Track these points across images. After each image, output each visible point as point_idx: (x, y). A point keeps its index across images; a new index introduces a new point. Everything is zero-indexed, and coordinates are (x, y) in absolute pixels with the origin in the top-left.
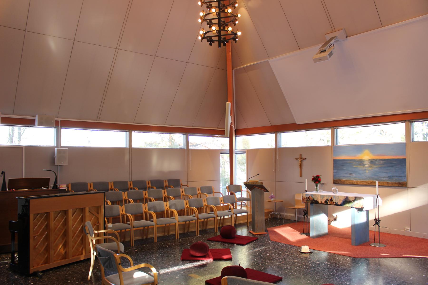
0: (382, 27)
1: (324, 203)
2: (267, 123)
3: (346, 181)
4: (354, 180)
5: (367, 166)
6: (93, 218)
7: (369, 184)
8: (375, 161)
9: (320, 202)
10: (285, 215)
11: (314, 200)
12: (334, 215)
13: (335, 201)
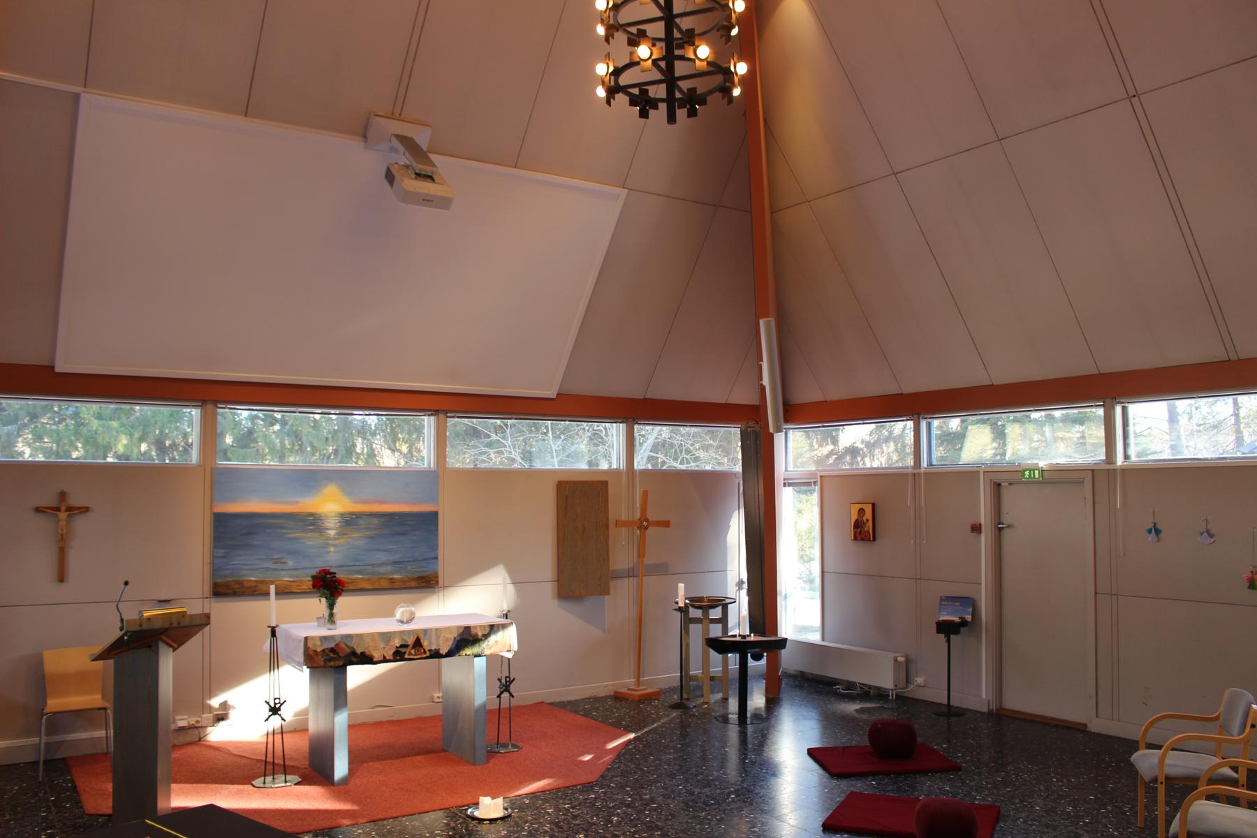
0: (515, 167)
1: (392, 658)
3: (259, 585)
4: (290, 577)
5: (332, 533)
8: (357, 518)
11: (354, 653)
12: (215, 702)
13: (430, 644)
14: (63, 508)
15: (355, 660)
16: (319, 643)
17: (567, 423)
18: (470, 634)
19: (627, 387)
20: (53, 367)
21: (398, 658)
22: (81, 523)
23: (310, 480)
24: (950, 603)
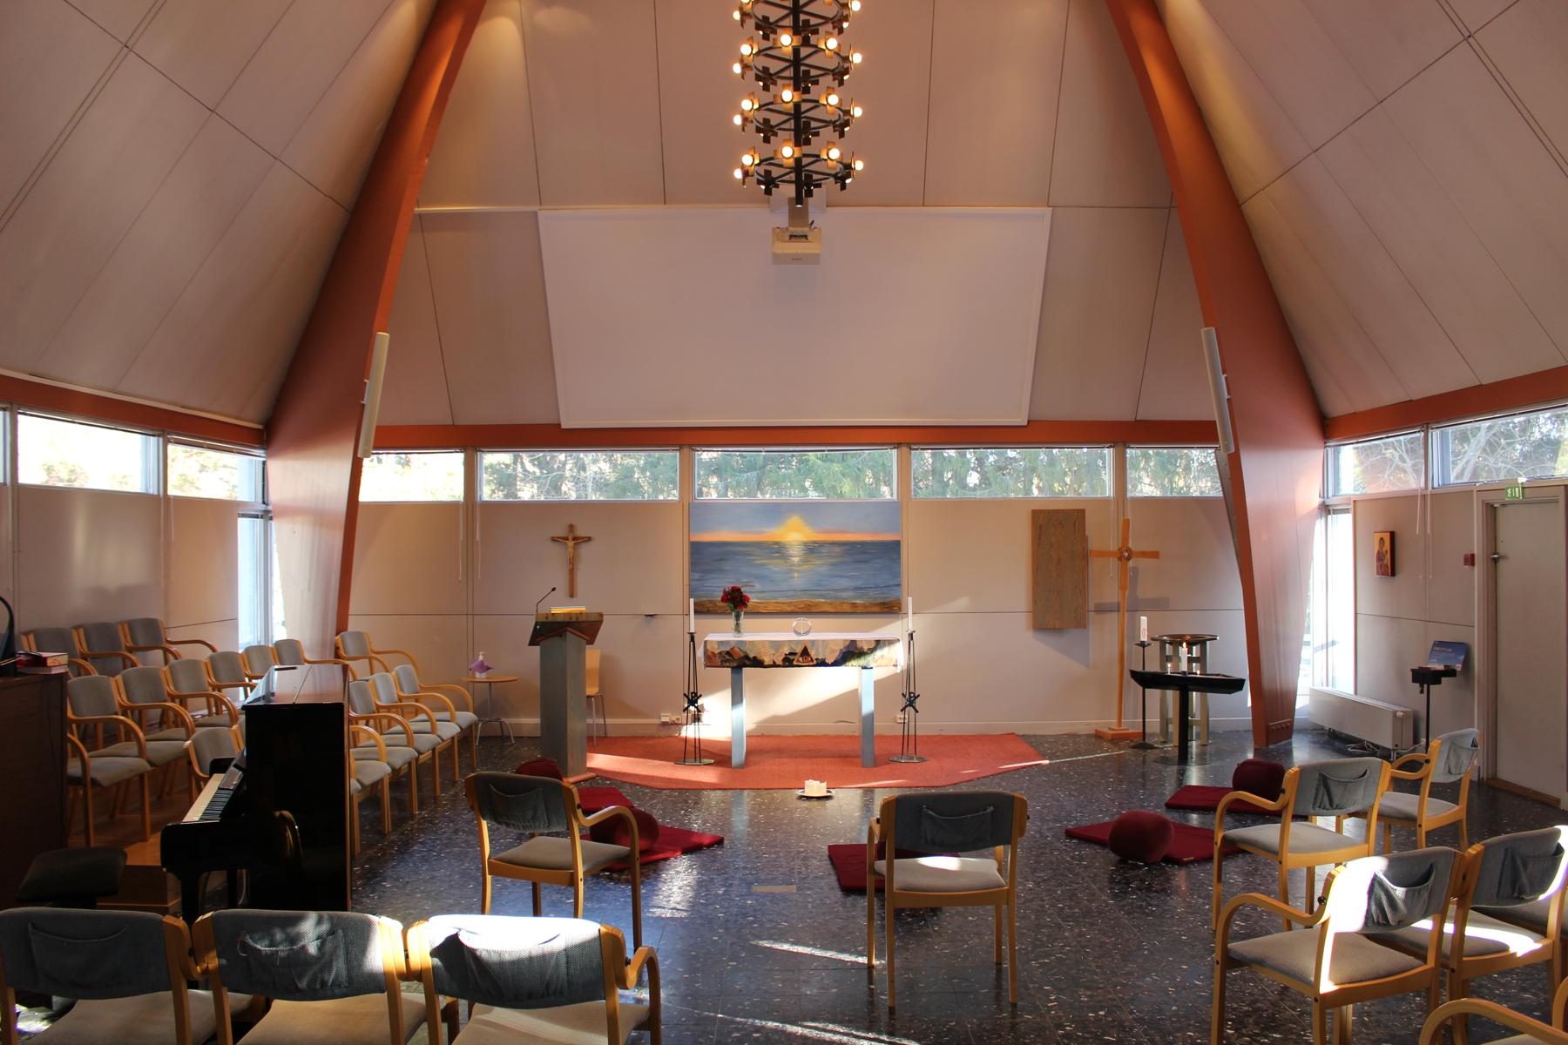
0: (923, 205)
1: (781, 663)
2: (438, 415)
4: (759, 599)
5: (796, 560)
6: (71, 795)
7: (800, 610)
9: (767, 661)
10: (510, 724)
11: (747, 657)
14: (570, 538)
15: (747, 662)
16: (716, 646)
17: (982, 450)
18: (856, 648)
19: (1120, 411)
20: (560, 425)
21: (787, 664)
22: (585, 549)
23: (776, 512)
24: (1443, 649)
